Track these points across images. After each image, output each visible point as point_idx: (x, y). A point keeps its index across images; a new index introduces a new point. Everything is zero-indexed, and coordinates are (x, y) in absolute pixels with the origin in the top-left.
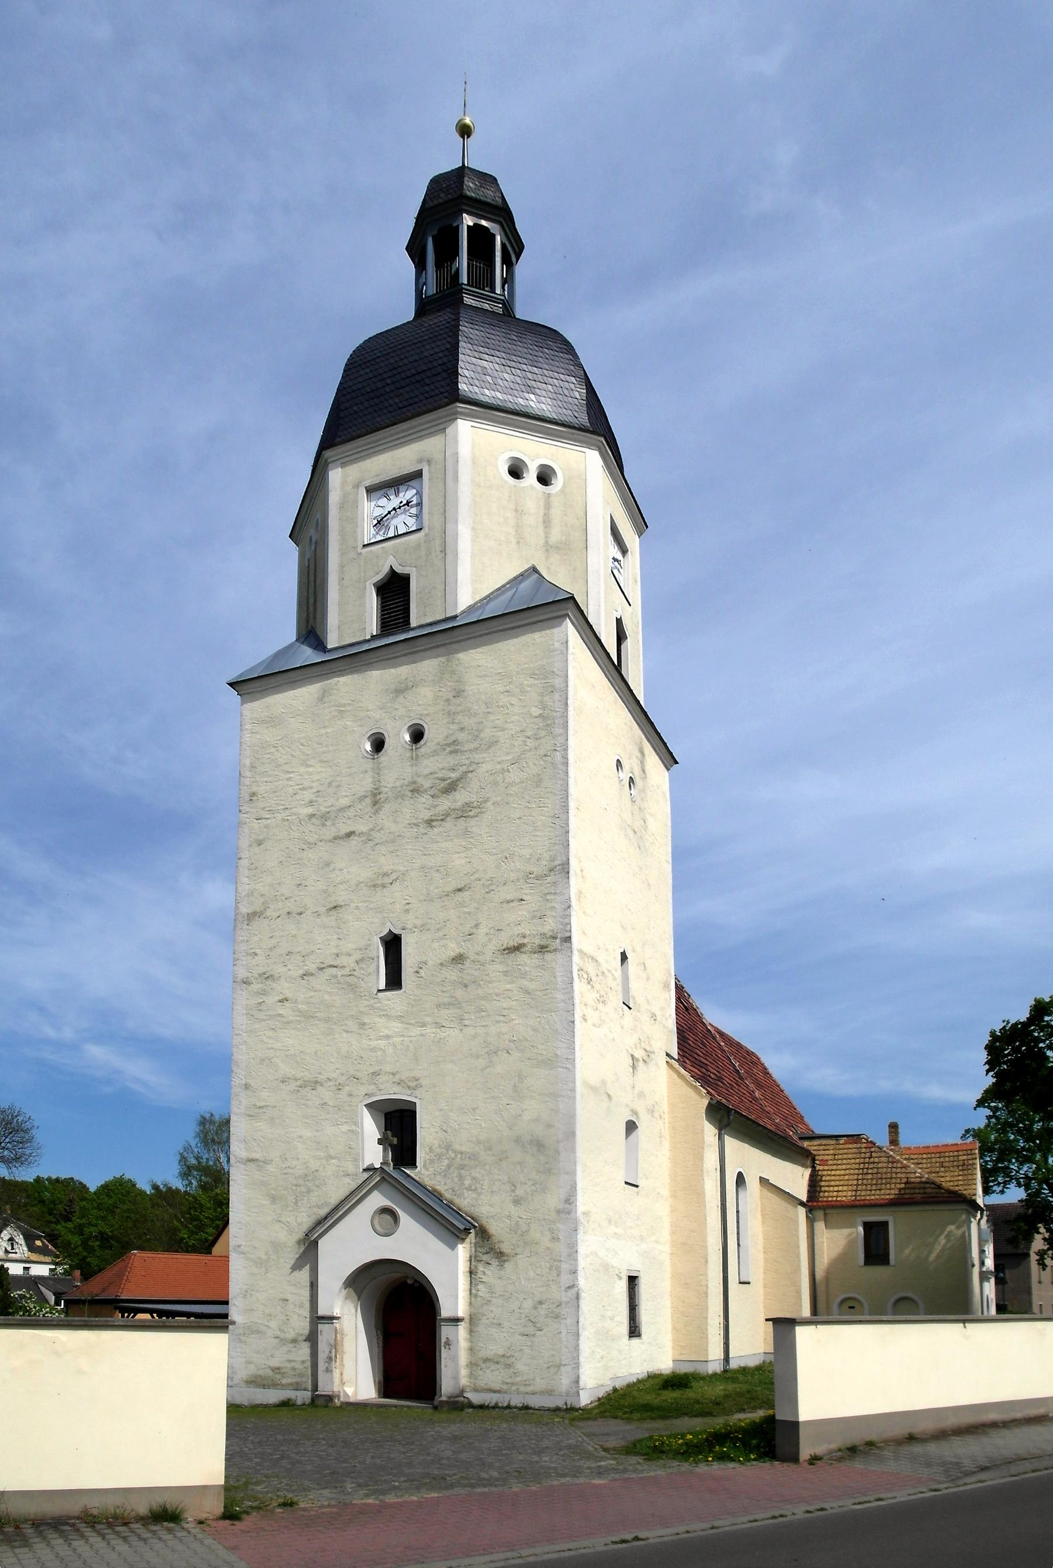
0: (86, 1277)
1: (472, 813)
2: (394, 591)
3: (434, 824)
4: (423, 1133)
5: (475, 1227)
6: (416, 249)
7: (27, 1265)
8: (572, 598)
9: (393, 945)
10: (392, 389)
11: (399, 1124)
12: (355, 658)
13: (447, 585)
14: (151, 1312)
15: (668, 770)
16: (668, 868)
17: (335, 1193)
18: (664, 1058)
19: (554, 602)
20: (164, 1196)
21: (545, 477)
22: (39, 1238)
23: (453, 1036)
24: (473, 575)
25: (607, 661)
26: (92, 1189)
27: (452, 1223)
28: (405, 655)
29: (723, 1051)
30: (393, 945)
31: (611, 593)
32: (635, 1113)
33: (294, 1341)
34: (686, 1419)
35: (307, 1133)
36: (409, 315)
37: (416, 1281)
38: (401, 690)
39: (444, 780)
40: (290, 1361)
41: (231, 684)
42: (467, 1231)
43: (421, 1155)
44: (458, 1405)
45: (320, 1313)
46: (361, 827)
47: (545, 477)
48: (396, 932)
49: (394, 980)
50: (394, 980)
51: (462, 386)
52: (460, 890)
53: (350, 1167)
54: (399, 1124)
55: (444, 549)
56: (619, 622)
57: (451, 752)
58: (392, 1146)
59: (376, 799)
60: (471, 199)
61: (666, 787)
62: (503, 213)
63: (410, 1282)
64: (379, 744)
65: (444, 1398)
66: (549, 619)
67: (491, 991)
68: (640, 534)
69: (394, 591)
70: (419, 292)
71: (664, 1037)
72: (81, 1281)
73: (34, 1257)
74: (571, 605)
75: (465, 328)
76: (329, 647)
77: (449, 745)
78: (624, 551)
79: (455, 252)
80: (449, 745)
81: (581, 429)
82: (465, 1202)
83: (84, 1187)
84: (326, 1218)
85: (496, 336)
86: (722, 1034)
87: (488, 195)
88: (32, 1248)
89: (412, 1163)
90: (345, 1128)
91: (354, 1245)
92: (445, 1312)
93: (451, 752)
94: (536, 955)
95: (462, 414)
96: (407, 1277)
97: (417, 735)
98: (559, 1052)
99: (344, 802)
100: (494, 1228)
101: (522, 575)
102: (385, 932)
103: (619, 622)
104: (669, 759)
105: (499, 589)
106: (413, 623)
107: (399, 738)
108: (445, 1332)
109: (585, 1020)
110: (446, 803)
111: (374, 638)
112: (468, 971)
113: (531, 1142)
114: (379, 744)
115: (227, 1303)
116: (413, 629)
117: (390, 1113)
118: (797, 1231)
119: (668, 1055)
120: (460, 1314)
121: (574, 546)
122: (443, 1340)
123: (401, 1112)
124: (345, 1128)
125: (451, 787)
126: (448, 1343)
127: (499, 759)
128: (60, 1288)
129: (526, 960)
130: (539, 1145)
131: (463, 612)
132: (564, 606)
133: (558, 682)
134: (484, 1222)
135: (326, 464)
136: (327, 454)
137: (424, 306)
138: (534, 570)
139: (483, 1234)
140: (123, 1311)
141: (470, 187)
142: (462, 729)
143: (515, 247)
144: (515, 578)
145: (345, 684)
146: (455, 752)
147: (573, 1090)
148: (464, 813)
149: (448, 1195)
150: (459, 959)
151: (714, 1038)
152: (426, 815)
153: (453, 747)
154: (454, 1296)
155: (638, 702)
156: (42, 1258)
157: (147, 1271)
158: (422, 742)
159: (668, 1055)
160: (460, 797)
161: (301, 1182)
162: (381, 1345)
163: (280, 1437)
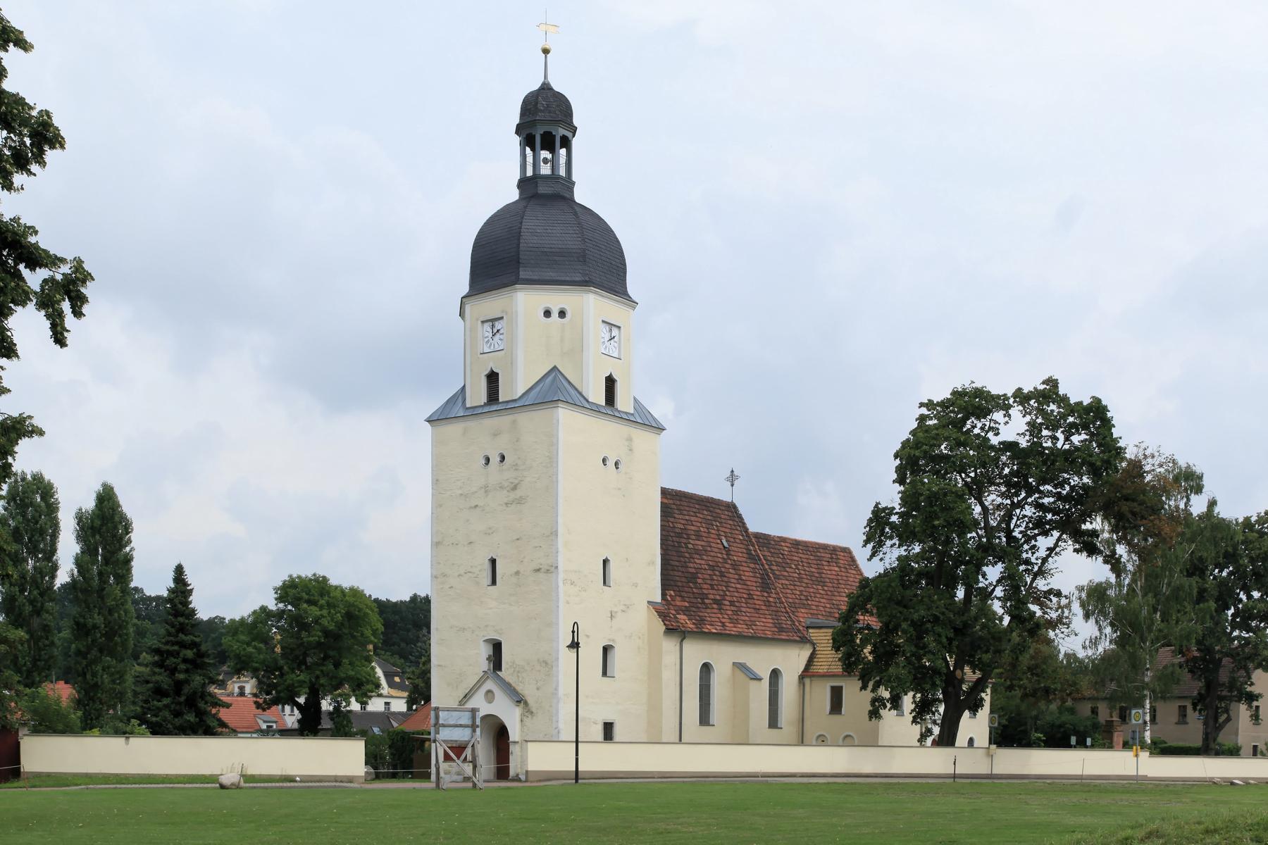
21: (562, 314)
26: (1072, 402)
27: (520, 700)
30: (493, 562)
34: (76, 548)
38: (496, 434)
46: (480, 504)
47: (562, 314)
49: (494, 582)
50: (494, 582)
55: (512, 363)
59: (486, 489)
82: (519, 688)
92: (511, 739)
97: (503, 458)
99: (474, 489)
107: (495, 459)
110: (513, 495)
114: (488, 460)
118: (1212, 784)
125: (515, 488)
129: (541, 575)
138: (555, 368)
139: (526, 703)
145: (472, 424)
148: (520, 501)
150: (517, 573)
152: (506, 500)
153: (515, 467)
160: (518, 493)
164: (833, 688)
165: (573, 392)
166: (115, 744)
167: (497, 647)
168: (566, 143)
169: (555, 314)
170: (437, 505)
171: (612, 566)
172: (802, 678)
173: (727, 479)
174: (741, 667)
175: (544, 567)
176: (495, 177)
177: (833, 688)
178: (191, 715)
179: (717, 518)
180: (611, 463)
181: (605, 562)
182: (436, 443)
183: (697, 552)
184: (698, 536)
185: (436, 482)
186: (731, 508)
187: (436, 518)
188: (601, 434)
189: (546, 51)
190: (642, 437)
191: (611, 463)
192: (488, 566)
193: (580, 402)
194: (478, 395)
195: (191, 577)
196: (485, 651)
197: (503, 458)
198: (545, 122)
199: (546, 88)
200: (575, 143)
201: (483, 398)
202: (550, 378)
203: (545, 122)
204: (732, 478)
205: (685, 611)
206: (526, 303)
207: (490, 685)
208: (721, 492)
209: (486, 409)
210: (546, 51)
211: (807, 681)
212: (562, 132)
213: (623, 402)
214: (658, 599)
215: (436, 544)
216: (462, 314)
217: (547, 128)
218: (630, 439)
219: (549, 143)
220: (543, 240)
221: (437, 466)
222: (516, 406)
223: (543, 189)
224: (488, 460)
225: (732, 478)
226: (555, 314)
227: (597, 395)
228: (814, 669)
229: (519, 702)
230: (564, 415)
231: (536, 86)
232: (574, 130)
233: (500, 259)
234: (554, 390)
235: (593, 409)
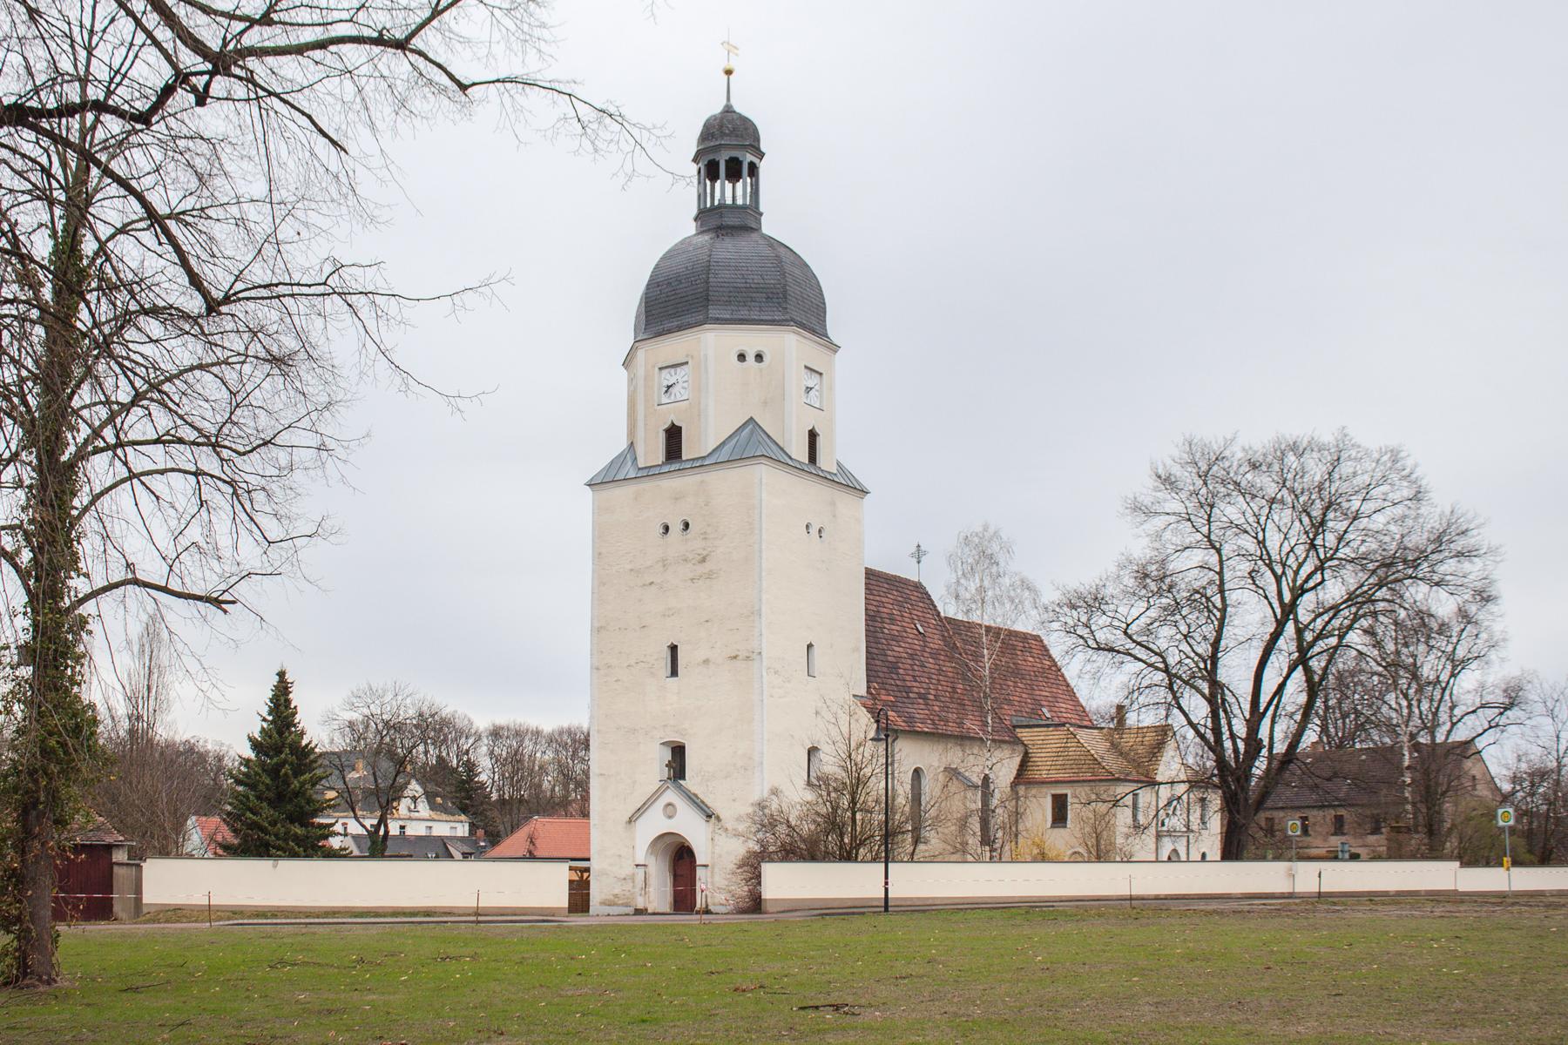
2: (674, 436)
12: (649, 473)
47: (759, 357)
49: (674, 673)
50: (674, 673)
59: (664, 563)
69: (674, 436)
88: (433, 806)
89: (683, 778)
97: (687, 525)
99: (649, 563)
107: (676, 527)
110: (701, 569)
114: (667, 529)
125: (703, 560)
148: (710, 576)
150: (706, 661)
160: (708, 566)
164: (1054, 797)
165: (774, 447)
166: (492, 899)
167: (678, 751)
168: (753, 171)
169: (750, 358)
170: (601, 582)
171: (816, 651)
172: (1015, 784)
173: (912, 555)
174: (953, 773)
175: (743, 654)
176: (667, 213)
177: (1054, 797)
178: (310, 844)
179: (907, 599)
180: (814, 530)
181: (810, 646)
182: (599, 510)
183: (894, 638)
184: (893, 620)
185: (598, 556)
186: (918, 587)
187: (598, 599)
188: (805, 496)
189: (729, 72)
190: (844, 500)
191: (814, 530)
192: (667, 654)
193: (781, 459)
194: (653, 450)
195: (289, 677)
197: (687, 525)
198: (728, 150)
199: (728, 110)
200: (764, 167)
201: (660, 456)
202: (747, 430)
203: (728, 150)
204: (919, 554)
205: (893, 706)
206: (714, 344)
207: (671, 796)
208: (908, 571)
209: (666, 469)
210: (729, 72)
211: (1022, 790)
212: (749, 158)
213: (825, 462)
214: (863, 691)
215: (598, 630)
216: (627, 363)
217: (734, 154)
218: (833, 504)
219: (734, 172)
220: (728, 275)
221: (600, 534)
222: (700, 464)
223: (730, 220)
224: (667, 529)
225: (919, 554)
226: (750, 358)
227: (800, 452)
228: (1029, 775)
229: (709, 816)
230: (764, 474)
231: (717, 109)
232: (761, 155)
233: (675, 302)
234: (749, 444)
235: (797, 468)
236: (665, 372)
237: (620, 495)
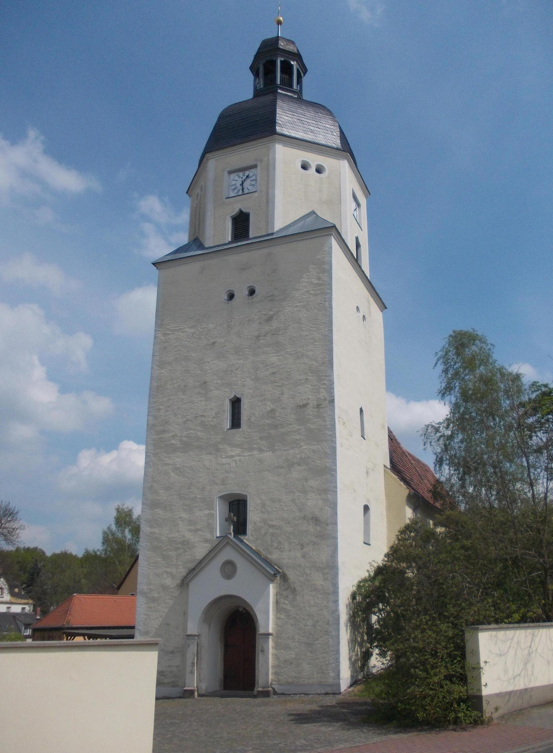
0: (44, 613)
1: (280, 333)
2: (241, 223)
3: (260, 338)
4: (251, 514)
5: (279, 572)
6: (254, 69)
7: (9, 606)
8: (334, 226)
9: (236, 403)
10: (245, 127)
11: (237, 507)
12: (220, 250)
13: (269, 217)
14: (83, 635)
15: (382, 311)
16: (383, 362)
17: (201, 551)
18: (382, 468)
19: (325, 228)
20: (90, 558)
21: (319, 170)
22: (16, 587)
23: (267, 455)
24: (285, 212)
25: (351, 257)
28: (247, 251)
29: (412, 464)
30: (236, 403)
31: (354, 225)
32: (368, 500)
33: (172, 652)
35: (184, 515)
36: (251, 96)
37: (244, 609)
39: (265, 315)
40: (170, 666)
41: (153, 264)
42: (275, 575)
43: (250, 527)
44: (266, 694)
45: (189, 633)
48: (239, 396)
50: (236, 423)
51: (278, 129)
52: (274, 373)
53: (209, 536)
54: (237, 507)
55: (268, 202)
56: (357, 239)
57: (270, 301)
58: (233, 521)
60: (282, 49)
61: (381, 320)
62: (298, 56)
63: (241, 610)
64: (231, 296)
65: (260, 689)
66: (322, 236)
67: (289, 430)
68: (366, 197)
69: (241, 223)
70: (255, 87)
71: (383, 457)
72: (40, 616)
73: (13, 600)
74: (334, 229)
75: (279, 103)
76: (207, 246)
77: (269, 297)
78: (358, 205)
79: (274, 72)
80: (269, 297)
81: (337, 149)
83: (44, 553)
84: (194, 569)
85: (294, 106)
86: (409, 454)
87: (290, 48)
88: (12, 594)
89: (244, 532)
90: (206, 512)
91: (211, 586)
92: (261, 630)
93: (270, 301)
94: (315, 410)
95: (278, 140)
96: (239, 606)
97: (252, 292)
98: (328, 465)
100: (291, 575)
101: (307, 215)
102: (232, 396)
103: (357, 239)
104: (383, 306)
105: (295, 221)
106: (251, 236)
107: (241, 293)
108: (259, 643)
109: (342, 446)
111: (230, 243)
112: (278, 418)
113: (312, 518)
114: (231, 296)
115: (133, 628)
116: (251, 239)
117: (232, 502)
119: (385, 466)
120: (271, 631)
121: (335, 201)
122: (260, 648)
123: (239, 501)
124: (206, 512)
126: (263, 651)
127: (295, 305)
128: (28, 621)
130: (316, 520)
131: (277, 232)
132: (332, 229)
133: (326, 267)
134: (285, 570)
135: (208, 160)
136: (208, 155)
137: (257, 93)
138: (313, 212)
139: (284, 578)
140: (68, 635)
141: (282, 44)
142: (276, 289)
143: (304, 69)
144: (304, 216)
146: (272, 300)
147: (336, 487)
149: (263, 553)
151: (407, 456)
154: (268, 620)
155: (367, 277)
156: (19, 601)
157: (87, 607)
158: (254, 295)
159: (385, 466)
160: (275, 324)
161: (180, 546)
162: (223, 653)
163: (168, 721)
181: (361, 410)
196: (219, 511)
226: (313, 170)
236: (232, 176)
237: (188, 270)
